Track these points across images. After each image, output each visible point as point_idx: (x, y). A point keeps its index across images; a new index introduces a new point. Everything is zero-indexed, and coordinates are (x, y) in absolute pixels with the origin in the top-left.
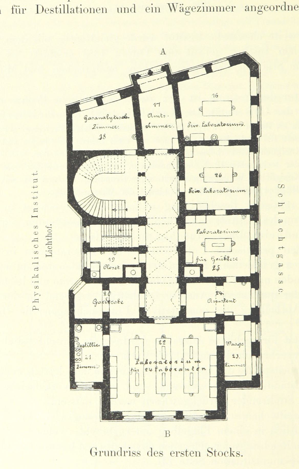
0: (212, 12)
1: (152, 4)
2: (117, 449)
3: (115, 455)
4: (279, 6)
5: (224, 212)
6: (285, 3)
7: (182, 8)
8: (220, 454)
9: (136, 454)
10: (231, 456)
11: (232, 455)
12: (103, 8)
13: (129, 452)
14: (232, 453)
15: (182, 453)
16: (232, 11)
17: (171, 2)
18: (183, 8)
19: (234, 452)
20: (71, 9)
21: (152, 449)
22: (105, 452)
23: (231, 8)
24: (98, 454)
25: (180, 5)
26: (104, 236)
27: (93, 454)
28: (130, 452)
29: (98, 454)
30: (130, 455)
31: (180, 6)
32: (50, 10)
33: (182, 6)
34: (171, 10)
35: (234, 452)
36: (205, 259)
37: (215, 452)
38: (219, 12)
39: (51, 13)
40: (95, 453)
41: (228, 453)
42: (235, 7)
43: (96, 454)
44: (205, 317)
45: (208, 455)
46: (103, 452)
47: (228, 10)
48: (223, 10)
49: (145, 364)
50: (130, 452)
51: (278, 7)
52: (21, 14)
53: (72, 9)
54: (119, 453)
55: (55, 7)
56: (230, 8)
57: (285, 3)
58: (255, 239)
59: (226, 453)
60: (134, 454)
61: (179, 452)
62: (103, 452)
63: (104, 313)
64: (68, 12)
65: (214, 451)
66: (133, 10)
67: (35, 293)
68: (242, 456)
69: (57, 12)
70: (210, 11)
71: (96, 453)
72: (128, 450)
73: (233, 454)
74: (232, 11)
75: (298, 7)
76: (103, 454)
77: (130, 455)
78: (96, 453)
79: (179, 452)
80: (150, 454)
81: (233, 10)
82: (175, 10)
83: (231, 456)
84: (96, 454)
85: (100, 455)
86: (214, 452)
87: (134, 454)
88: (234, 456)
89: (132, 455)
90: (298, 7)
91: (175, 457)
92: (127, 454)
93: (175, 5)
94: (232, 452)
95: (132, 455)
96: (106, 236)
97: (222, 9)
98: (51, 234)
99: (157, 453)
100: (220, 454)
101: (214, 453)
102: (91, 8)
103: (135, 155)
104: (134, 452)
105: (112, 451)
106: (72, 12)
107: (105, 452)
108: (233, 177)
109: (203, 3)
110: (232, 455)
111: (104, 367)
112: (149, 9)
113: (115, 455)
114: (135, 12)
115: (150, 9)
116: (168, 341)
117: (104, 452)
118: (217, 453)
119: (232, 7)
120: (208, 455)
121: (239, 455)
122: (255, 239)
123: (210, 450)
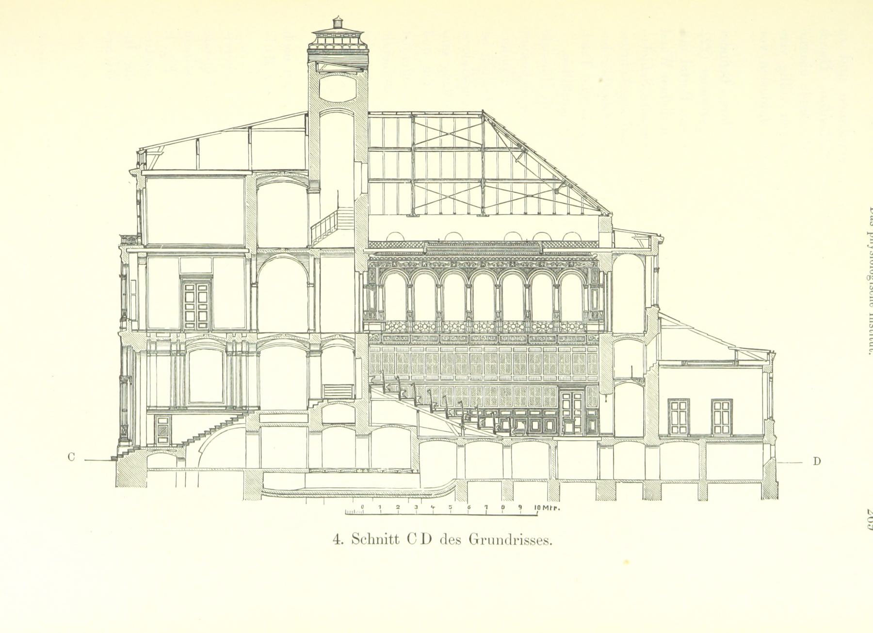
2: (506, 536)
3: (502, 544)
9: (530, 541)
13: (520, 540)
21: (511, 534)
22: (489, 539)
24: (480, 541)
26: (251, 329)
27: (474, 541)
28: (522, 539)
29: (480, 541)
30: (522, 544)
32: (455, 540)
39: (456, 543)
40: (476, 540)
41: (365, 539)
43: (477, 542)
45: (353, 542)
46: (486, 539)
49: (175, 456)
50: (522, 539)
54: (508, 541)
59: (363, 539)
60: (527, 541)
62: (486, 539)
68: (551, 544)
71: (477, 540)
72: (520, 537)
77: (522, 544)
78: (477, 540)
80: (443, 541)
84: (477, 542)
85: (482, 544)
87: (527, 541)
89: (525, 544)
91: (367, 545)
92: (518, 542)
95: (525, 544)
96: (251, 329)
98: (870, 300)
99: (453, 539)
103: (180, 269)
104: (527, 540)
105: (379, 537)
107: (489, 539)
108: (138, 264)
113: (502, 544)
116: (353, 401)
117: (487, 540)
120: (353, 542)
123: (356, 535)
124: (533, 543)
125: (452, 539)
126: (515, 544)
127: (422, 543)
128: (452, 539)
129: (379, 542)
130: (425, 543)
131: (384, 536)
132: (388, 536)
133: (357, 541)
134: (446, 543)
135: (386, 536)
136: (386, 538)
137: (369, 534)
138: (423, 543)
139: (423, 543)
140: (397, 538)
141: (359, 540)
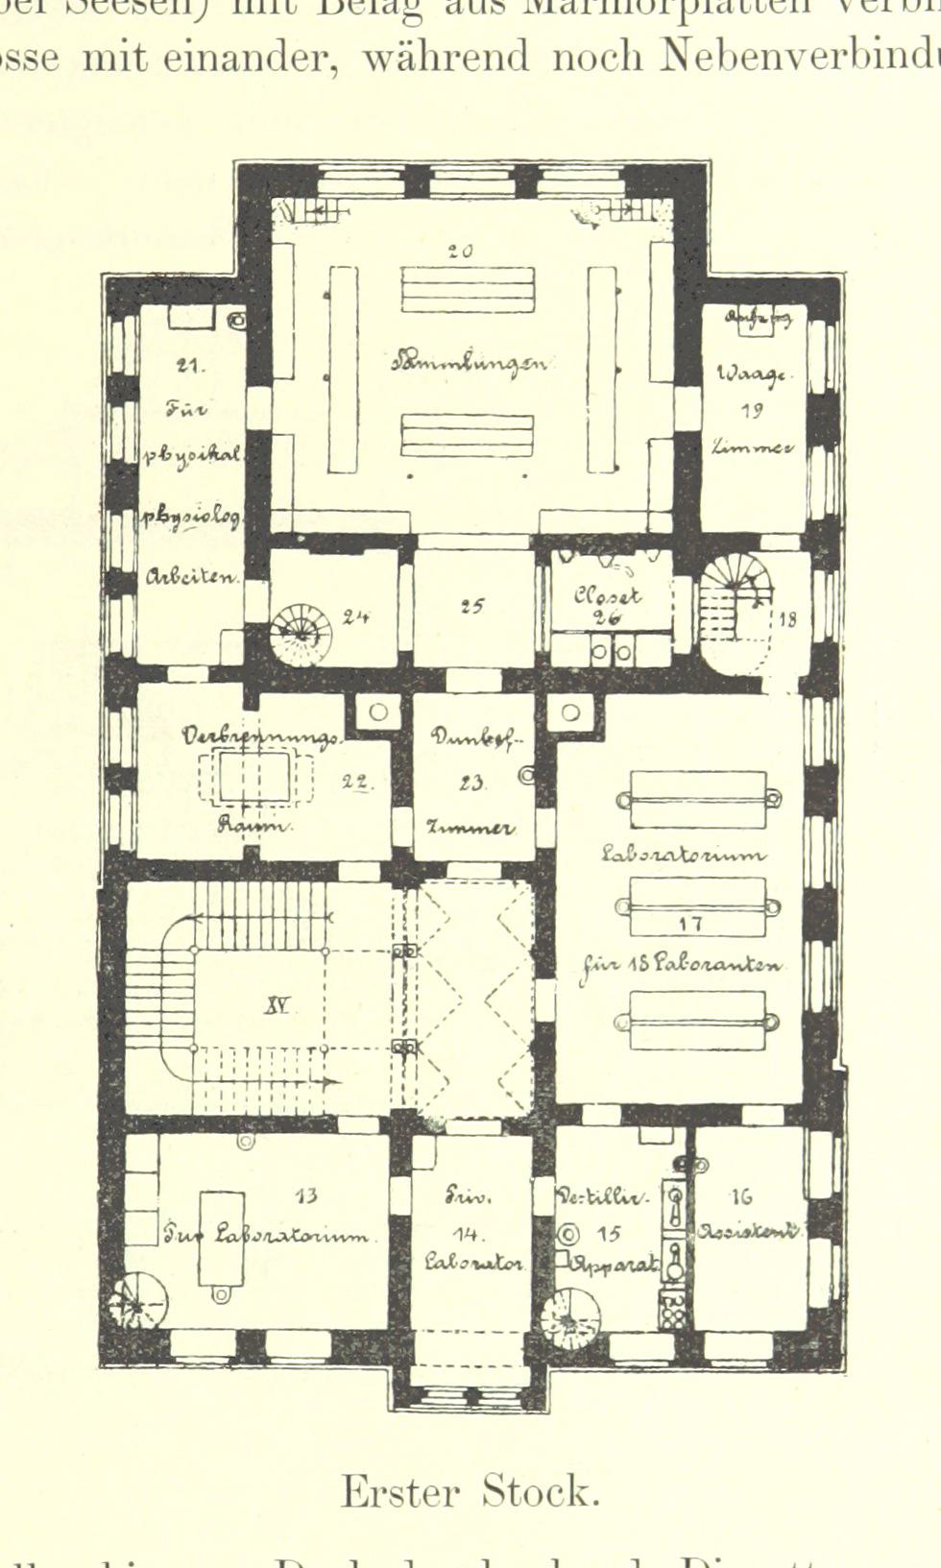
0: (106, 74)
1: (189, 40)
3: (501, 68)
4: (458, 55)
5: (547, 813)
6: (928, 38)
7: (406, 56)
8: (533, 1496)
9: (22, 59)
10: (572, 1503)
11: (576, 1500)
12: (765, 52)
14: (575, 1493)
15: (397, 1491)
16: (836, 67)
17: (373, 49)
18: (411, 56)
19: (583, 1488)
20: (225, 55)
23: (312, 57)
25: (402, 43)
31: (402, 48)
33: (406, 47)
34: (374, 67)
35: (583, 1488)
36: (613, 963)
37: (512, 1487)
38: (430, 73)
39: (134, 10)
42: (326, 55)
44: (668, 1130)
45: (485, 1501)
47: (299, 64)
48: (433, 66)
51: (453, 57)
52: (772, 70)
53: (230, 56)
54: (921, 58)
55: (135, 48)
56: (477, 58)
57: (928, 38)
58: (382, 1132)
59: (555, 1491)
61: (385, 1491)
63: (788, 1123)
64: (215, 68)
65: (510, 1483)
66: (517, 60)
67: (390, 53)
69: (142, 68)
70: (436, 68)
72: (183, 48)
73: (581, 1495)
74: (836, 67)
75: (56, 57)
76: (805, 61)
79: (385, 1491)
81: (320, 67)
82: (384, 66)
83: (572, 1503)
86: (509, 1490)
88: (583, 1504)
89: (492, 11)
90: (56, 57)
93: (385, 56)
94: (576, 1490)
95: (492, 11)
97: (107, 64)
99: (175, 57)
100: (533, 1496)
101: (507, 1492)
102: (250, 52)
104: (13, 55)
105: (250, 51)
106: (229, 65)
109: (125, 40)
110: (576, 1500)
111: (104, 1276)
112: (825, 56)
114: (524, 66)
115: (828, 55)
118: (519, 1493)
119: (316, 53)
120: (485, 1501)
121: (400, 1501)
122: (382, 1132)
123: (494, 1481)
124: (31, 65)
125: (300, 55)
126: (586, 12)
127: (345, 1503)
128: (300, 55)
129: (620, 9)
130: (328, 10)
131: (118, 48)
132: (131, 48)
133: (498, 1496)
134: (283, 67)
135: (125, 47)
136: (125, 54)
137: (626, 41)
138: (324, 11)
139: (324, 11)
140: (516, 1489)
141: (86, 3)
